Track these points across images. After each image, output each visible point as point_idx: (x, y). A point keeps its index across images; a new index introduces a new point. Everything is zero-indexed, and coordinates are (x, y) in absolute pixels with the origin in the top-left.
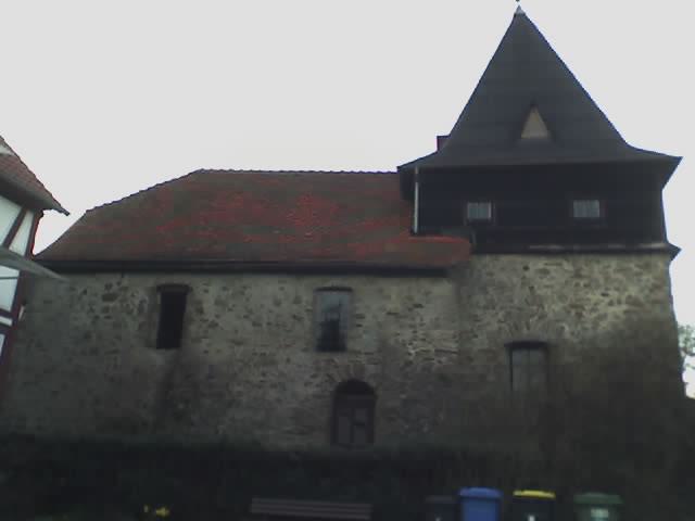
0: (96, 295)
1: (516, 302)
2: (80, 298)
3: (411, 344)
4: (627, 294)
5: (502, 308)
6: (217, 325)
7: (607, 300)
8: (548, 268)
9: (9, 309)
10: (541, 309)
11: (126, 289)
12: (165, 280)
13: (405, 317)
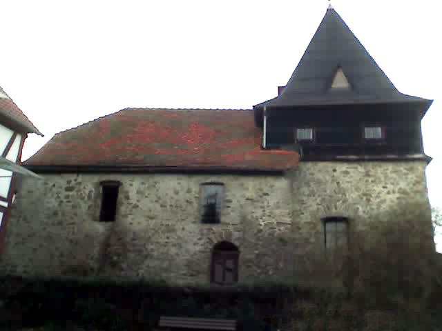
0: (61, 187)
2: (51, 190)
3: (261, 218)
6: (138, 206)
7: (386, 190)
8: (349, 170)
10: (344, 197)
12: (105, 178)
13: (258, 201)
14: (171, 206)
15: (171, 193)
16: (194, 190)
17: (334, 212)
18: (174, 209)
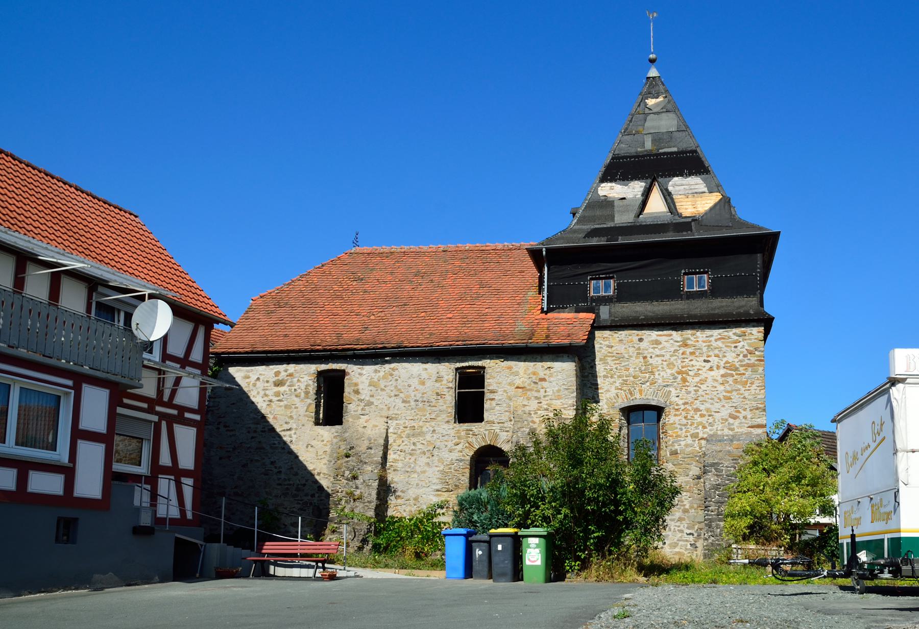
0: (267, 382)
1: (631, 370)
2: (254, 385)
3: (536, 413)
4: (725, 360)
5: (619, 377)
6: (372, 403)
7: (708, 365)
8: (659, 338)
9: (196, 408)
10: (652, 377)
11: (291, 375)
12: (323, 367)
13: (531, 390)
14: (416, 401)
15: (415, 382)
16: (446, 377)
17: (638, 399)
18: (421, 405)
